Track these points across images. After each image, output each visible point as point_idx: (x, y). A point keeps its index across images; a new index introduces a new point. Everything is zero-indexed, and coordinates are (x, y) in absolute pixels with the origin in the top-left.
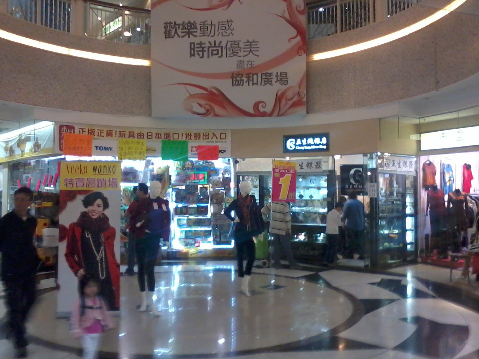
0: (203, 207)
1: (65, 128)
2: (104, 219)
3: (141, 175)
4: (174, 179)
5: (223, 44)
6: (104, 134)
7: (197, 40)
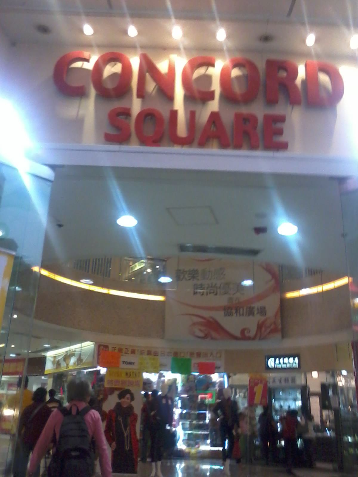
0: (202, 414)
1: (102, 347)
2: (131, 408)
3: (155, 387)
4: (180, 389)
5: (218, 285)
6: (129, 352)
7: (199, 283)
